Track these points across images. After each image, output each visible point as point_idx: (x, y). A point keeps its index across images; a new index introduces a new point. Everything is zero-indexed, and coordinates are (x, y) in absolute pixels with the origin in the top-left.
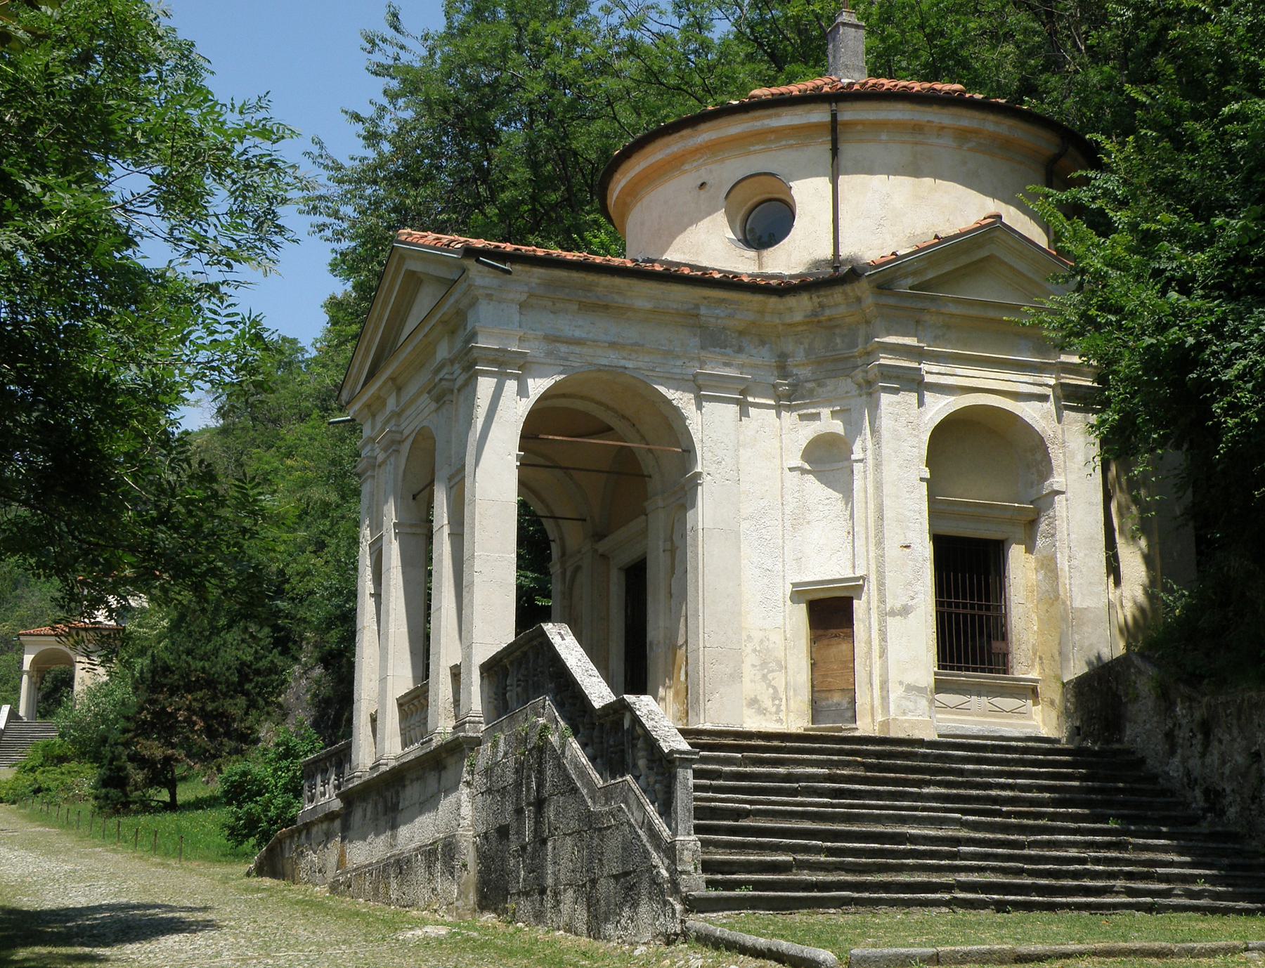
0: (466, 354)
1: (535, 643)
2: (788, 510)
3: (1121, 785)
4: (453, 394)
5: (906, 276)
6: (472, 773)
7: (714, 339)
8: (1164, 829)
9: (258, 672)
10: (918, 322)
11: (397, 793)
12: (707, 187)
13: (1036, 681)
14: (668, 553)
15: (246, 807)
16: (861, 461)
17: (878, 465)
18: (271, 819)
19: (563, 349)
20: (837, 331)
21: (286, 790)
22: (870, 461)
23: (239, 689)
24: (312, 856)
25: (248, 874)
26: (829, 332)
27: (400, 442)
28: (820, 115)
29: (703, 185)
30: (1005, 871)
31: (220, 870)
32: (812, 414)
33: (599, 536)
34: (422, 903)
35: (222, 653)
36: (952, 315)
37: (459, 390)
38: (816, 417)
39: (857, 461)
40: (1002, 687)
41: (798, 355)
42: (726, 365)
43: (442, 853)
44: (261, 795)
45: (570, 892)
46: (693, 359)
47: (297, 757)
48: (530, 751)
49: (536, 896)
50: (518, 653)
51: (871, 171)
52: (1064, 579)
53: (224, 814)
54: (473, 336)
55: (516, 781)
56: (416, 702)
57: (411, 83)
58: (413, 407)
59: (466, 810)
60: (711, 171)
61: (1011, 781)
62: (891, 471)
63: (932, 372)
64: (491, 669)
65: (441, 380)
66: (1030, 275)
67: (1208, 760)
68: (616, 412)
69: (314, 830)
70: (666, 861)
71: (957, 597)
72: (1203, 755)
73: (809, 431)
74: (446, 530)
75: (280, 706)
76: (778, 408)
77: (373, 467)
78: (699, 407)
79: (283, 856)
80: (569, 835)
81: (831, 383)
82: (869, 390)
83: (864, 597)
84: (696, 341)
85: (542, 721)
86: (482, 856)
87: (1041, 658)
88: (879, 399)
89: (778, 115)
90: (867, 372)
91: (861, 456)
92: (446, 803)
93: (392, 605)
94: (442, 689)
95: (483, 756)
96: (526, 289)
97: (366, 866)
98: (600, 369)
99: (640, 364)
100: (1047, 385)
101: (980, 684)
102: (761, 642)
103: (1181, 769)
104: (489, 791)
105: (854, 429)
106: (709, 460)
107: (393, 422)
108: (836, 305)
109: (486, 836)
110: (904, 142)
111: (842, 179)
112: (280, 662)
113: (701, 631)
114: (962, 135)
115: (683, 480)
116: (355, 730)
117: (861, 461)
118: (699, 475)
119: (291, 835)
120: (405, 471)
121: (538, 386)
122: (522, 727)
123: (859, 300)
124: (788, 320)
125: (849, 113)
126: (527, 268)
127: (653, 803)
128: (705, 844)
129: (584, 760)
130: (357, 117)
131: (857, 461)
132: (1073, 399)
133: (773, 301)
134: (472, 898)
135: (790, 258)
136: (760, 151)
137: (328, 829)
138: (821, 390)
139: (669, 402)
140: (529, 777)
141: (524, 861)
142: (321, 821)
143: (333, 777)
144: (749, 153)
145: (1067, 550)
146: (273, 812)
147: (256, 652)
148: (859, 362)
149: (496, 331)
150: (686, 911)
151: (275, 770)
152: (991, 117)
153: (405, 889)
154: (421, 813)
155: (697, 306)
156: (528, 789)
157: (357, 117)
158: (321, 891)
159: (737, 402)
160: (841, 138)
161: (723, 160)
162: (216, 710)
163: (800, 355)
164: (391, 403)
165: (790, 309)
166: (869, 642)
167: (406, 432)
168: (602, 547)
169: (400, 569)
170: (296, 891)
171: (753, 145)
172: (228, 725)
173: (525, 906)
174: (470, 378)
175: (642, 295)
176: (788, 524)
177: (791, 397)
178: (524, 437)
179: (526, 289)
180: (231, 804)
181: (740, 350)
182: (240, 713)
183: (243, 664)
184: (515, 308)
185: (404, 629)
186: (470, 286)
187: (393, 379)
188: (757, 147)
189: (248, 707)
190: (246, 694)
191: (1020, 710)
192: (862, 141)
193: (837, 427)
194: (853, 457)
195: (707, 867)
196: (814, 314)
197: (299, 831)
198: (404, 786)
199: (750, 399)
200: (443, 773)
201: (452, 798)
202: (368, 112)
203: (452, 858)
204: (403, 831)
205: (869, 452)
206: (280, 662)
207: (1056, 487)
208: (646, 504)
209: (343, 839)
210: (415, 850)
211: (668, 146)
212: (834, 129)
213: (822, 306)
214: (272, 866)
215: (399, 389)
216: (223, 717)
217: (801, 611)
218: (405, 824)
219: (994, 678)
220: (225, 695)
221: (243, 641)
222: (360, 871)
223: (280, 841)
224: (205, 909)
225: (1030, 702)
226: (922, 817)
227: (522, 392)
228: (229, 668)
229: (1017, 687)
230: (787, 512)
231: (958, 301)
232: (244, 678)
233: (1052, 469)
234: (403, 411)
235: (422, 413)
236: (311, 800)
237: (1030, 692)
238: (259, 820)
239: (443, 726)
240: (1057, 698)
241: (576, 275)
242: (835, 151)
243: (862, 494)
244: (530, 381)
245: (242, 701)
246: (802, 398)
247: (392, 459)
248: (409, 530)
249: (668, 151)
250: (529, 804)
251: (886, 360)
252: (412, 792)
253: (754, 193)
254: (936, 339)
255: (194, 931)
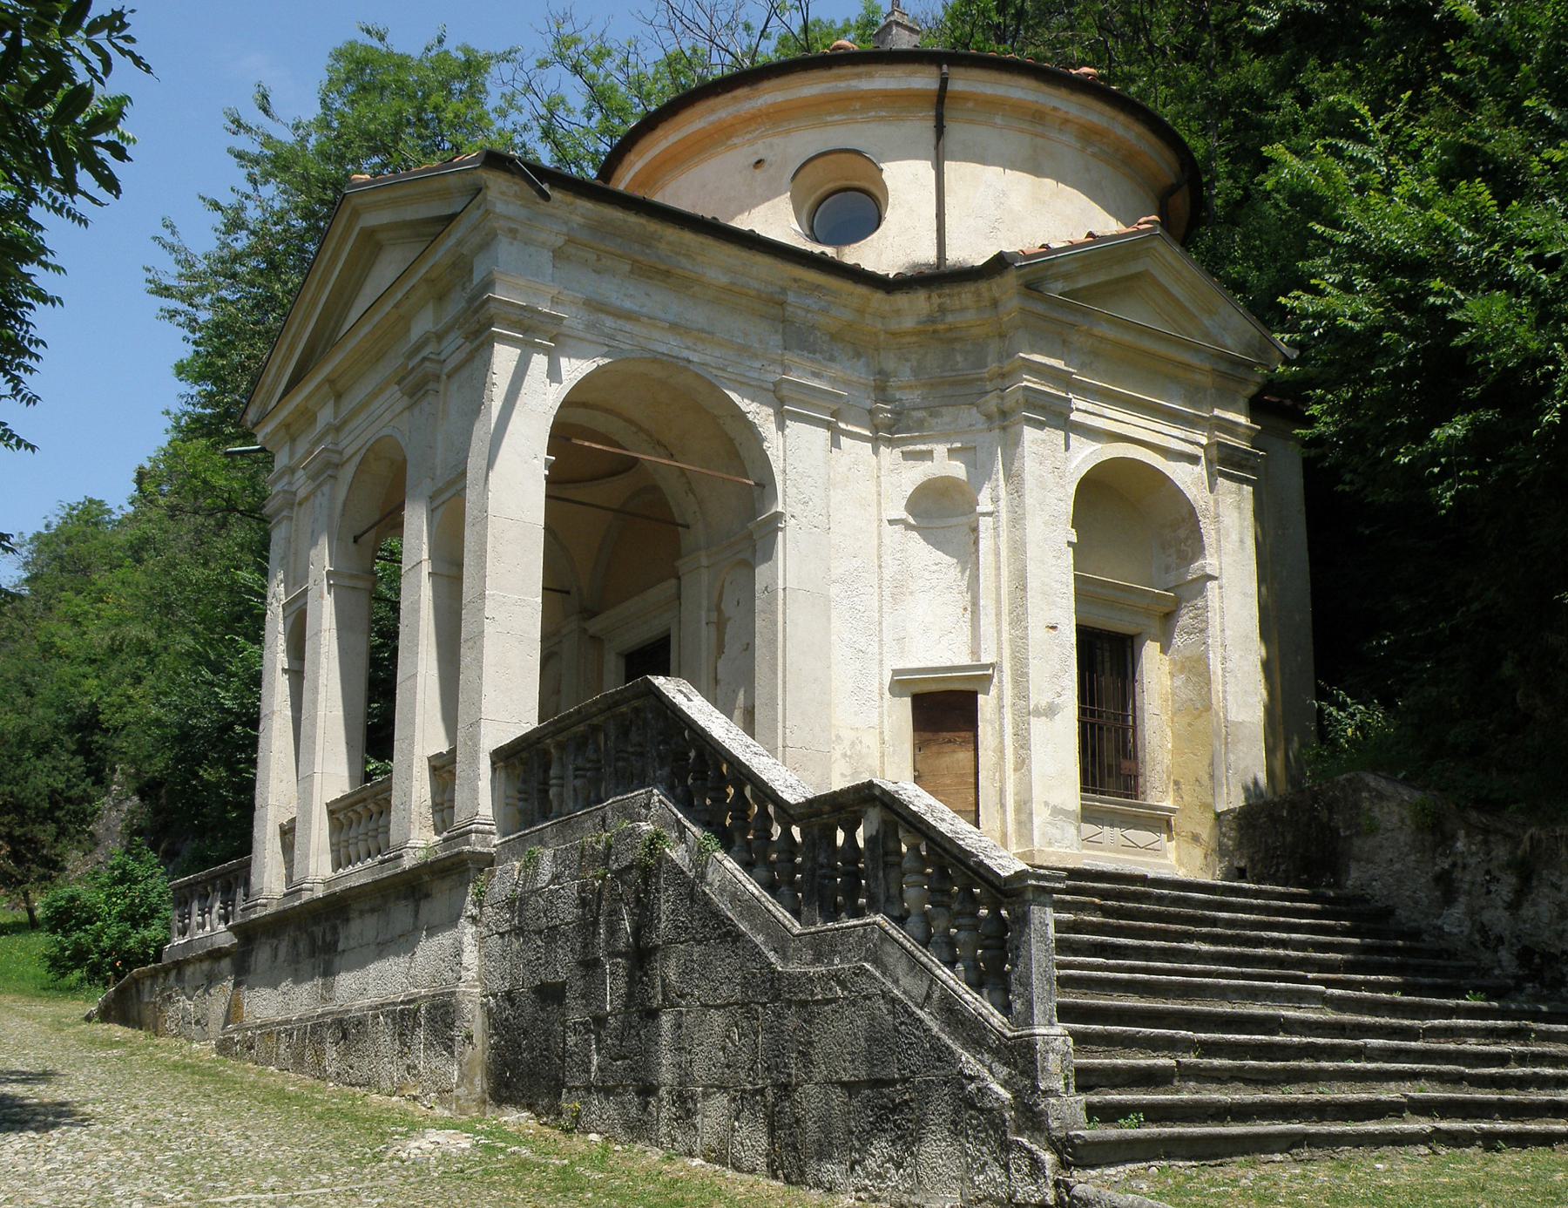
0: (476, 312)
1: (624, 709)
2: (887, 574)
3: (1400, 943)
4: (444, 378)
5: (1056, 278)
6: (479, 904)
7: (799, 338)
8: (1544, 1008)
9: (69, 800)
10: (1064, 341)
11: (335, 929)
12: (766, 165)
13: (1173, 811)
14: (713, 628)
15: (76, 935)
16: (990, 514)
17: (1017, 520)
18: (103, 950)
19: (609, 322)
20: (958, 346)
21: (121, 917)
22: (1004, 516)
23: (47, 816)
24: (184, 1003)
25: (88, 1019)
26: (950, 351)
27: (337, 466)
28: (923, 80)
29: (759, 163)
30: (1441, 1078)
31: (47, 1009)
32: (921, 452)
33: (588, 613)
34: (386, 1084)
35: (31, 778)
36: (1102, 339)
37: (449, 377)
38: (927, 455)
39: (984, 514)
40: (1136, 816)
41: (903, 374)
42: (816, 375)
43: (439, 1016)
44: (92, 923)
45: (720, 1101)
46: (773, 362)
47: (135, 882)
48: (619, 874)
49: (631, 1097)
50: (581, 728)
51: (983, 161)
52: (1217, 686)
53: (41, 942)
54: (488, 284)
55: (582, 918)
56: (359, 808)
57: (279, 163)
58: (363, 416)
59: (471, 957)
60: (771, 146)
61: (1285, 935)
62: (1035, 527)
63: (1082, 409)
64: (505, 757)
65: (424, 359)
66: (1187, 304)
67: (1527, 911)
68: (650, 436)
69: (189, 971)
70: (1003, 1071)
71: (1092, 704)
72: (1513, 907)
73: (915, 474)
74: (426, 568)
75: (92, 835)
76: (876, 442)
77: (291, 506)
78: (781, 427)
79: (140, 1001)
80: (717, 1007)
81: (948, 414)
82: (1004, 422)
83: (993, 691)
84: (777, 339)
85: (646, 827)
86: (496, 1023)
87: (1176, 783)
88: (1019, 435)
89: (870, 76)
90: (1002, 398)
91: (990, 508)
92: (430, 949)
93: (322, 680)
94: (414, 788)
95: (507, 878)
96: (565, 229)
97: (279, 1024)
98: (657, 359)
99: (708, 359)
100: (1198, 444)
101: (1114, 812)
102: (853, 744)
103: (1468, 923)
104: (518, 931)
105: (980, 472)
106: (789, 498)
107: (329, 439)
108: (964, 309)
109: (509, 996)
110: (1022, 131)
111: (949, 166)
112: (93, 791)
113: (780, 725)
114: (1088, 135)
115: (751, 526)
116: (255, 845)
117: (990, 514)
118: (779, 516)
119: (154, 975)
120: (345, 505)
121: (575, 369)
122: (593, 838)
123: (995, 304)
124: (894, 327)
125: (964, 82)
126: (569, 198)
127: (951, 964)
128: (1081, 1039)
129: (753, 888)
130: (217, 206)
131: (984, 514)
132: (1227, 462)
133: (878, 296)
134: (480, 1084)
135: (889, 250)
136: (842, 123)
137: (211, 970)
138: (934, 421)
139: (742, 416)
140: (614, 912)
141: (598, 1041)
142: (200, 959)
143: (218, 905)
144: (826, 124)
145: (1220, 650)
146: (106, 943)
147: (68, 780)
148: (989, 387)
149: (521, 282)
150: (1064, 1165)
151: (109, 896)
152: (1122, 117)
153: (353, 1060)
154: (380, 955)
155: (784, 290)
156: (613, 931)
157: (217, 206)
158: (203, 1050)
159: (828, 426)
160: (947, 114)
161: (788, 132)
162: (25, 835)
163: (906, 374)
164: (326, 416)
165: (898, 312)
166: (1001, 750)
167: (349, 451)
168: (594, 626)
169: (334, 633)
170: (168, 1048)
171: (830, 114)
172: (36, 851)
173: (602, 1109)
174: (477, 349)
175: (718, 261)
176: (886, 593)
177: (893, 427)
178: (553, 436)
179: (565, 229)
180: (55, 933)
181: (832, 359)
182: (51, 839)
183: (54, 791)
184: (546, 257)
185: (338, 712)
186: (487, 212)
187: (330, 381)
188: (836, 117)
189: (58, 834)
190: (56, 821)
191: (1155, 846)
192: (971, 122)
193: (958, 470)
194: (979, 509)
195: (1086, 1080)
196: (931, 319)
197: (166, 970)
198: (348, 920)
199: (842, 425)
200: (425, 907)
201: (445, 939)
202: (227, 200)
203: (451, 1026)
204: (346, 982)
205: (1002, 503)
206: (93, 791)
207: (1209, 571)
208: (678, 563)
209: (237, 985)
210: (370, 1008)
211: (713, 111)
212: (941, 100)
213: (942, 310)
214: (121, 1010)
215: (339, 396)
216: (32, 843)
217: (903, 709)
218: (349, 970)
219: (1129, 805)
220: (34, 822)
221: (54, 768)
222: (268, 1030)
223: (136, 981)
224: (45, 1076)
225: (1164, 836)
226: (1280, 991)
227: (554, 374)
228: (39, 794)
229: (1152, 817)
230: (886, 576)
231: (1115, 322)
232: (55, 805)
233: (1203, 548)
234: (345, 422)
235: (381, 414)
236: (183, 933)
237: (1161, 823)
238: (89, 951)
239: (417, 838)
240: (1206, 831)
241: (633, 220)
242: (940, 130)
243: (991, 558)
244: (564, 361)
245: (52, 828)
246: (908, 430)
247: (326, 489)
248: (347, 582)
249: (713, 118)
250: (613, 954)
251: (1029, 381)
252: (360, 928)
253: (825, 178)
254: (1082, 367)
255: (45, 1127)
